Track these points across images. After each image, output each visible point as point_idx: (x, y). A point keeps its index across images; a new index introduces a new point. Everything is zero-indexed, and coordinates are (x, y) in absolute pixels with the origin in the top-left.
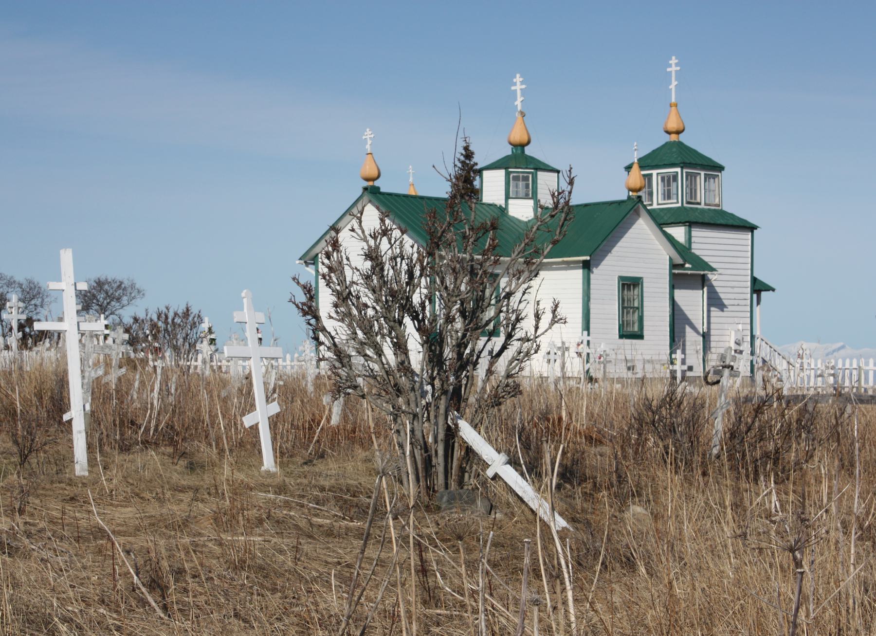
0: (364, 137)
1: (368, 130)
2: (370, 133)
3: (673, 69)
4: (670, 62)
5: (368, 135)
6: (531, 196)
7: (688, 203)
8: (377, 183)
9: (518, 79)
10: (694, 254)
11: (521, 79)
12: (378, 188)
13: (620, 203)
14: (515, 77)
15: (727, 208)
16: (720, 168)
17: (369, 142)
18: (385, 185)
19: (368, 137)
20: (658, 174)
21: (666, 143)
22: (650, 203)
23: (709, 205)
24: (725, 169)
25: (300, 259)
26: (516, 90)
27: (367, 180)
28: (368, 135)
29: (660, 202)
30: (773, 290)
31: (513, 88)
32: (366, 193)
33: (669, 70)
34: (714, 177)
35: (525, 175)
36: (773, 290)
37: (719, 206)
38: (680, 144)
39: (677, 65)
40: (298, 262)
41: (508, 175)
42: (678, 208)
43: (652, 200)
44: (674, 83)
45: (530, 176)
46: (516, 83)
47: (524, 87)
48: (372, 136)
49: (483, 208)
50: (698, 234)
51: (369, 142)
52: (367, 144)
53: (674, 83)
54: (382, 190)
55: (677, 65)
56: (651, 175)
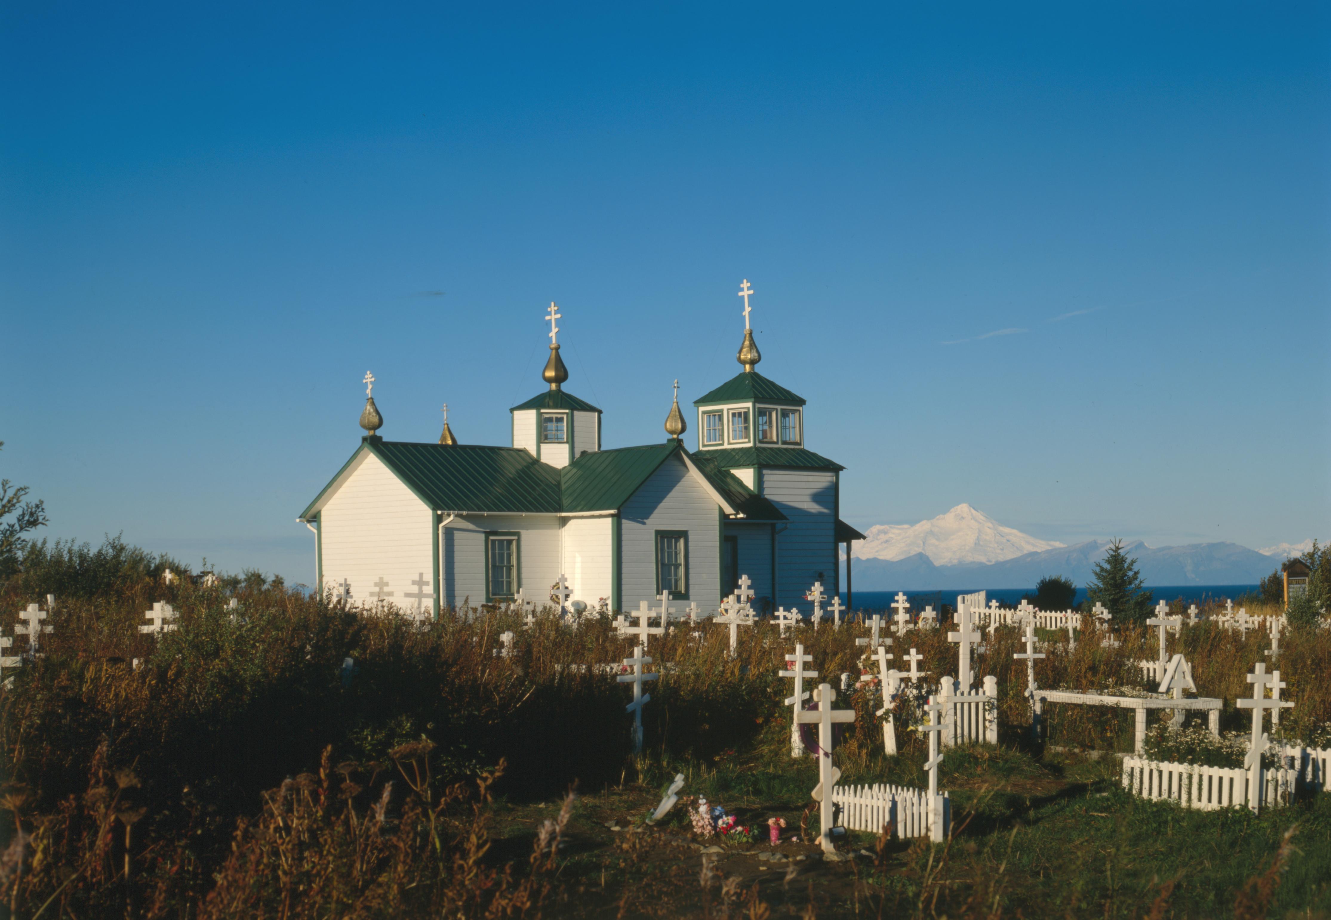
0: (364, 381)
1: (368, 372)
2: (371, 376)
3: (553, 317)
4: (742, 286)
5: (369, 378)
6: (565, 440)
7: (761, 442)
8: (379, 432)
9: (745, 284)
10: (766, 499)
11: (749, 284)
12: (380, 438)
13: (662, 446)
14: (743, 283)
15: (810, 446)
16: (801, 402)
17: (370, 387)
18: (388, 434)
19: (369, 380)
20: (728, 410)
21: (740, 375)
22: (721, 442)
23: (784, 443)
24: (807, 403)
25: (300, 517)
26: (743, 297)
27: (370, 429)
28: (369, 378)
29: (706, 443)
30: (864, 538)
31: (740, 294)
32: (366, 444)
33: (547, 318)
34: (794, 412)
35: (559, 416)
36: (864, 538)
37: (799, 444)
38: (754, 376)
39: (749, 289)
40: (298, 520)
41: (539, 415)
42: (750, 448)
43: (723, 440)
44: (748, 309)
45: (565, 416)
46: (551, 312)
47: (751, 292)
48: (373, 379)
49: (519, 455)
50: (773, 478)
51: (370, 387)
52: (367, 388)
53: (748, 309)
54: (385, 439)
55: (749, 289)
56: (722, 411)
